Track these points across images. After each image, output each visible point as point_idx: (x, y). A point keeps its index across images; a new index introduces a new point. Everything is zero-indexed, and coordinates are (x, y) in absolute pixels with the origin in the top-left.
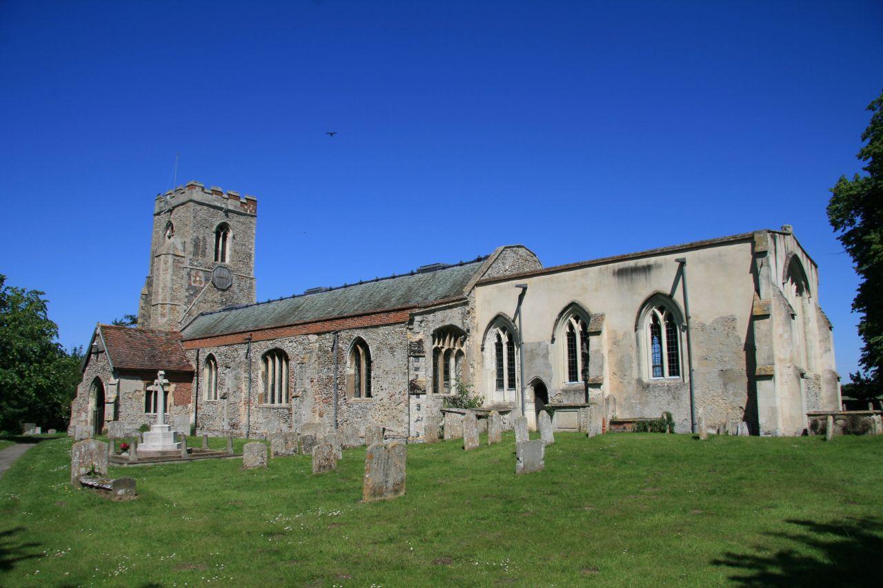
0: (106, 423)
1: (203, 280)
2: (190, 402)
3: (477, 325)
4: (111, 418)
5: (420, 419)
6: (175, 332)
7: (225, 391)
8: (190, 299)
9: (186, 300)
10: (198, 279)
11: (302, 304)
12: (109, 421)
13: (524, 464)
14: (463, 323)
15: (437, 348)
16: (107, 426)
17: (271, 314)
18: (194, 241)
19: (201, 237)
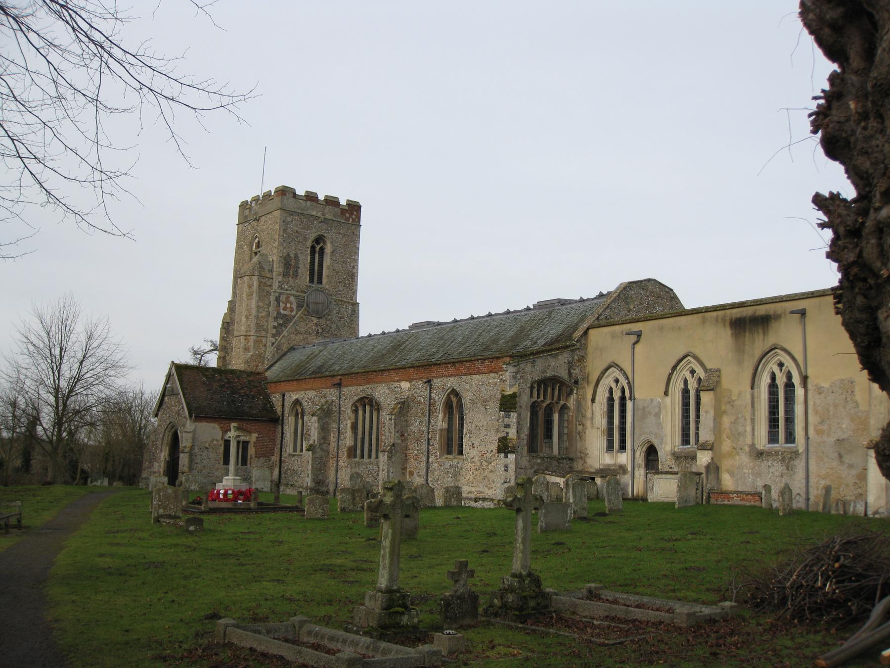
0: (180, 474)
1: (294, 306)
2: (273, 455)
3: (588, 376)
4: (186, 469)
5: (508, 481)
6: (258, 373)
7: (311, 442)
8: (279, 329)
9: (274, 331)
10: (288, 305)
11: (404, 342)
12: (183, 473)
13: (546, 524)
14: (570, 374)
15: (534, 403)
16: (182, 478)
17: (369, 353)
18: (285, 259)
19: (292, 255)
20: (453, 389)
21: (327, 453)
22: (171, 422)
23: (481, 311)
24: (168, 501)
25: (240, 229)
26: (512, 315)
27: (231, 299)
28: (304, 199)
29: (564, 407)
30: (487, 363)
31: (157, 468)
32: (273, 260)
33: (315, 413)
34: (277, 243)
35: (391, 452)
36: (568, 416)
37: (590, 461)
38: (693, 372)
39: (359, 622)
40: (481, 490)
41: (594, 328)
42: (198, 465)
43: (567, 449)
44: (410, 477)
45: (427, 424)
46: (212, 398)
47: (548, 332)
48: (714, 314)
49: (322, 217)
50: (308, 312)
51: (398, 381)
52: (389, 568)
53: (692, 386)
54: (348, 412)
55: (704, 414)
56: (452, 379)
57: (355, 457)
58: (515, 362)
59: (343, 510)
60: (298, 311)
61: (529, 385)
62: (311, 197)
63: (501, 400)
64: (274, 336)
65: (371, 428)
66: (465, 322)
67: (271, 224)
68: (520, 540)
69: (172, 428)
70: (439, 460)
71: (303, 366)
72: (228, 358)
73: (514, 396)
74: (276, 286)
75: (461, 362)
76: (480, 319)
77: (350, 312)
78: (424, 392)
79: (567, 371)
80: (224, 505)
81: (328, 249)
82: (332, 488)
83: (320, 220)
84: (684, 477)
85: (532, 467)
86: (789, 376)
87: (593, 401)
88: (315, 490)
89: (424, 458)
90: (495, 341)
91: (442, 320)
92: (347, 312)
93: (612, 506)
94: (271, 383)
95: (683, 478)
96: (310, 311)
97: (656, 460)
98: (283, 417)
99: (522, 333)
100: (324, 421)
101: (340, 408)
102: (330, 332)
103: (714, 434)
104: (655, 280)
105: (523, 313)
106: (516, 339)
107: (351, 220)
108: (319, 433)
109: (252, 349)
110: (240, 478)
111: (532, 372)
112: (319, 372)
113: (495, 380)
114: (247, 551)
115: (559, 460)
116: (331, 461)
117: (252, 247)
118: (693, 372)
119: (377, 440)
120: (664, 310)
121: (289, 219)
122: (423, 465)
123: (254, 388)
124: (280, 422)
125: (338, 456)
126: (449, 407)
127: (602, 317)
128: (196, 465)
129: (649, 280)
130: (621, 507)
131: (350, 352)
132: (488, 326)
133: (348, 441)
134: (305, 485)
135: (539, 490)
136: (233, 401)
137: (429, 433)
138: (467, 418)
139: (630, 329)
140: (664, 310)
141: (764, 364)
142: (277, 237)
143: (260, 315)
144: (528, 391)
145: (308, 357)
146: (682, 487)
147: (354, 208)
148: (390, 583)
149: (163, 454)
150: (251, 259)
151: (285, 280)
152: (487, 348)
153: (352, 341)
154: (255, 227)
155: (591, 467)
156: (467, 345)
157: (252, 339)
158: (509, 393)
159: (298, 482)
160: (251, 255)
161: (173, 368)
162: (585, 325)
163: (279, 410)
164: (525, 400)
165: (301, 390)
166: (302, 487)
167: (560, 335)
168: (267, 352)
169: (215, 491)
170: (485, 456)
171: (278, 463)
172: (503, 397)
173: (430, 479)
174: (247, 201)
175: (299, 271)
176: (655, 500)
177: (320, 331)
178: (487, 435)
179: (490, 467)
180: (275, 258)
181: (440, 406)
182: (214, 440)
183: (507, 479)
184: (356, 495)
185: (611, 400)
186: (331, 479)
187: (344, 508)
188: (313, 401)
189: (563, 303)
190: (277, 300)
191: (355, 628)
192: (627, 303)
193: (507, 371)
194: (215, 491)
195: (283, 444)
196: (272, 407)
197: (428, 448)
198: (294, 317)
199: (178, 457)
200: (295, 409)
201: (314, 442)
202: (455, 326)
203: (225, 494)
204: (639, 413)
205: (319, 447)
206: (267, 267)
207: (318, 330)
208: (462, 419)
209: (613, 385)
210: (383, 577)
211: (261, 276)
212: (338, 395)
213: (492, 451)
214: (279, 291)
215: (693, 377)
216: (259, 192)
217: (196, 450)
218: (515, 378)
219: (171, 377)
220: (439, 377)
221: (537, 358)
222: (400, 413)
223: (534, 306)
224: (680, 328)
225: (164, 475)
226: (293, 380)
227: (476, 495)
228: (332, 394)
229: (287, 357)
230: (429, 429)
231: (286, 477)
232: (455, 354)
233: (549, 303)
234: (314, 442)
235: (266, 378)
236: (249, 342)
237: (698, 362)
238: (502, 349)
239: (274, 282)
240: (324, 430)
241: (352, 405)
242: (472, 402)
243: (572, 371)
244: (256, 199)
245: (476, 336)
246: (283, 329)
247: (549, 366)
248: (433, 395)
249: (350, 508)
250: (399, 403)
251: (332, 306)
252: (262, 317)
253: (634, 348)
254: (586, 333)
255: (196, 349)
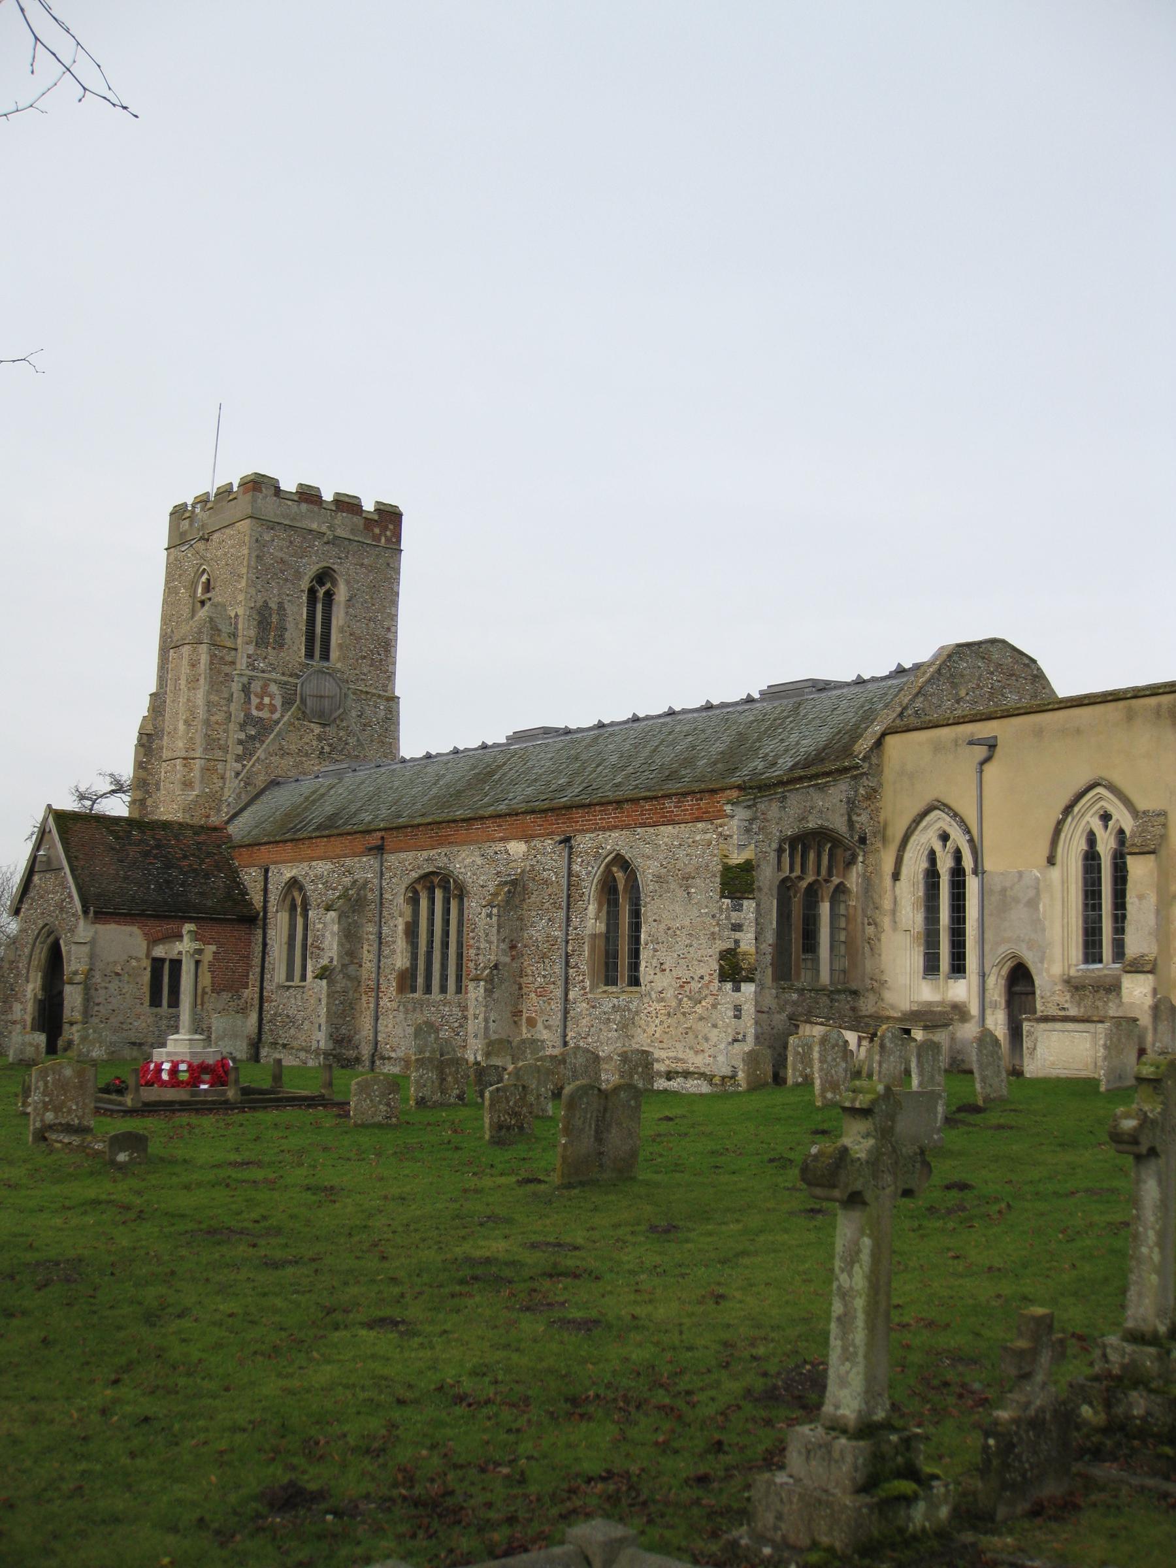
0: (66, 1027)
1: (278, 702)
3: (885, 828)
4: (77, 1016)
6: (215, 829)
7: (324, 962)
8: (248, 746)
9: (239, 750)
11: (500, 767)
12: (72, 1024)
14: (851, 824)
15: (784, 881)
16: (72, 1033)
17: (430, 789)
19: (274, 606)
20: (618, 855)
21: (356, 984)
22: (47, 924)
23: (652, 706)
24: (65, 1094)
25: (172, 557)
26: (718, 712)
27: (154, 690)
28: (296, 498)
29: (841, 889)
30: (689, 802)
31: (19, 1014)
32: (236, 615)
33: (331, 906)
34: (243, 583)
35: (492, 980)
36: (847, 907)
37: (888, 996)
38: (1106, 817)
39: (776, 1528)
40: (681, 1056)
41: (897, 732)
42: (101, 1008)
43: (844, 971)
44: (529, 1031)
45: (564, 925)
46: (126, 878)
47: (797, 743)
48: (1153, 701)
49: (329, 533)
50: (303, 712)
51: (502, 839)
52: (866, 1357)
53: (1106, 846)
54: (398, 902)
55: (1136, 900)
56: (615, 834)
57: (414, 990)
58: (749, 800)
59: (421, 1102)
60: (285, 711)
61: (775, 846)
62: (308, 495)
63: (723, 875)
64: (239, 759)
65: (446, 933)
66: (655, 721)
67: (233, 546)
68: (1152, 1236)
69: (48, 936)
70: (589, 996)
71: (298, 815)
72: (149, 802)
73: (748, 867)
74: (242, 663)
75: (634, 801)
76: (652, 722)
77: (383, 713)
78: (556, 861)
79: (846, 818)
80: (171, 1094)
81: (341, 593)
82: (366, 1051)
83: (325, 539)
84: (1117, 1028)
85: (782, 1009)
86: (958, 856)
87: (896, 876)
88: (335, 1056)
89: (559, 993)
90: (689, 762)
91: (573, 726)
92: (376, 713)
93: (988, 1090)
94: (241, 846)
95: (1114, 1030)
96: (308, 711)
97: (1027, 994)
98: (265, 913)
99: (742, 746)
100: (350, 920)
101: (381, 895)
102: (345, 752)
103: (1157, 940)
104: (1003, 642)
105: (739, 708)
106: (731, 759)
107: (383, 540)
108: (341, 944)
109: (197, 785)
110: (201, 1037)
111: (780, 819)
112: (331, 827)
113: (708, 836)
114: (264, 1218)
115: (832, 994)
116: (364, 998)
117: (195, 591)
118: (1106, 817)
119: (460, 956)
120: (1020, 699)
121: (267, 537)
122: (557, 1006)
123: (207, 857)
124: (260, 923)
125: (378, 988)
126: (608, 889)
127: (910, 712)
128: (96, 1008)
129: (993, 641)
130: (1005, 1092)
131: (391, 788)
132: (670, 733)
133: (400, 959)
134: (314, 1046)
135: (829, 1058)
136: (167, 882)
137: (567, 942)
138: (649, 911)
139: (972, 734)
140: (1020, 699)
141: (802, 856)
142: (244, 570)
143: (213, 719)
144: (773, 856)
145: (307, 798)
146: (1113, 1048)
147: (389, 518)
148: (867, 1403)
149: (30, 986)
150: (193, 613)
151: (259, 652)
152: (672, 776)
153: (394, 767)
154: (202, 552)
155: (893, 1007)
156: (630, 770)
157: (198, 765)
158: (738, 862)
159: (297, 1039)
160: (193, 607)
161: (51, 820)
162: (878, 728)
163: (257, 899)
164: (767, 876)
165: (301, 861)
166: (307, 1050)
167: (824, 749)
168: (226, 790)
169: (152, 1066)
170: (687, 988)
171: (256, 1002)
172: (727, 869)
173: (570, 1034)
174: (185, 504)
175: (287, 635)
176: (1041, 1074)
177: (327, 749)
178: (691, 946)
179: (699, 1009)
180: (240, 611)
181: (590, 887)
182: (131, 958)
183: (738, 1033)
184: (447, 1070)
185: (932, 874)
186: (364, 1033)
187: (423, 1098)
188: (327, 882)
189: (822, 686)
190: (246, 690)
191: (767, 1551)
192: (954, 686)
193: (733, 816)
194: (152, 1066)
195: (266, 965)
196: (244, 893)
197: (567, 973)
198: (277, 722)
199: (61, 993)
200: (289, 898)
201: (331, 961)
202: (601, 735)
203: (174, 1071)
204: (993, 900)
205: (341, 971)
206: (225, 628)
207: (323, 748)
208: (636, 914)
209: (937, 846)
210: (843, 1383)
211: (214, 645)
212: (378, 869)
213: (702, 977)
214: (247, 672)
215: (1106, 827)
216: (209, 486)
217: (97, 978)
218: (748, 831)
219: (47, 836)
220: (586, 831)
221: (788, 791)
222: (508, 902)
223: (762, 693)
224: (1078, 731)
225: (33, 1029)
226: (286, 841)
227: (668, 1066)
228: (364, 868)
229: (264, 798)
230: (567, 934)
231: (272, 1030)
232: (607, 787)
233: (782, 688)
234: (331, 961)
235: (229, 837)
236: (191, 770)
237: (1120, 799)
238: (704, 776)
239: (239, 655)
240: (350, 936)
241: (407, 888)
242: (659, 879)
243: (855, 818)
244: (203, 500)
245: (646, 753)
246: (258, 745)
247: (812, 808)
248: (576, 868)
249: (435, 1098)
250: (506, 883)
251: (349, 702)
252: (217, 723)
253: (981, 772)
254: (879, 743)
255: (82, 789)
